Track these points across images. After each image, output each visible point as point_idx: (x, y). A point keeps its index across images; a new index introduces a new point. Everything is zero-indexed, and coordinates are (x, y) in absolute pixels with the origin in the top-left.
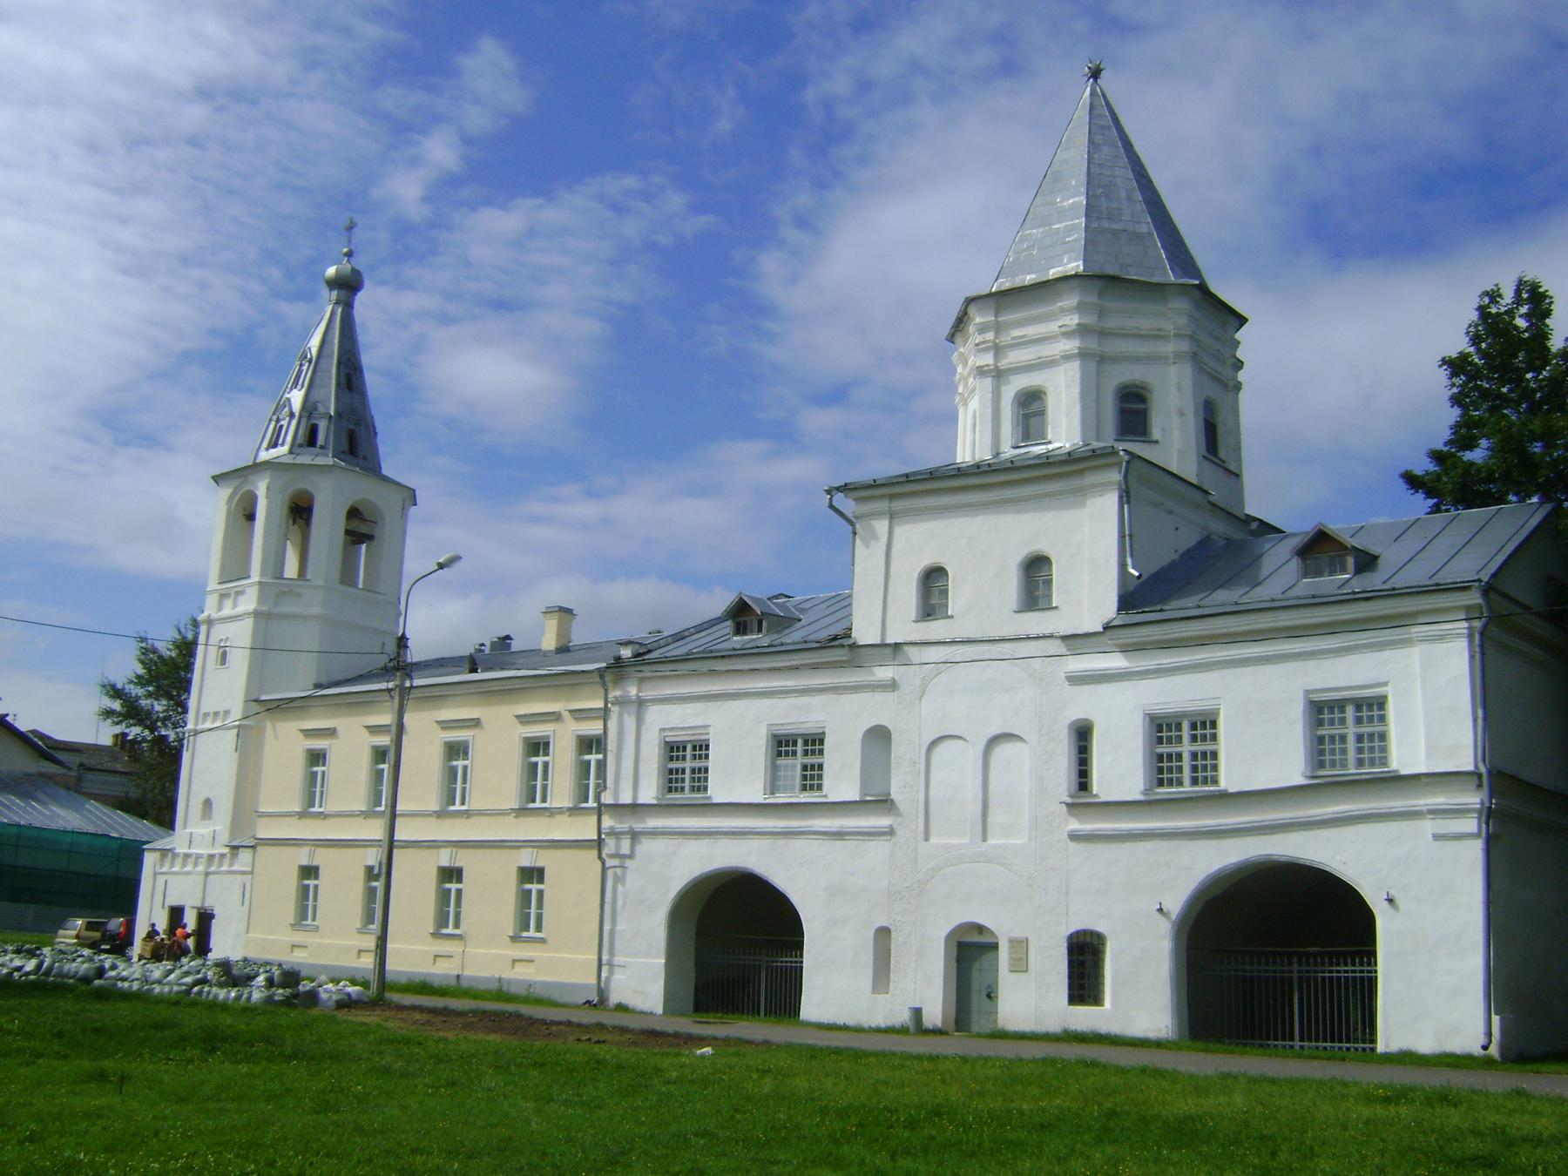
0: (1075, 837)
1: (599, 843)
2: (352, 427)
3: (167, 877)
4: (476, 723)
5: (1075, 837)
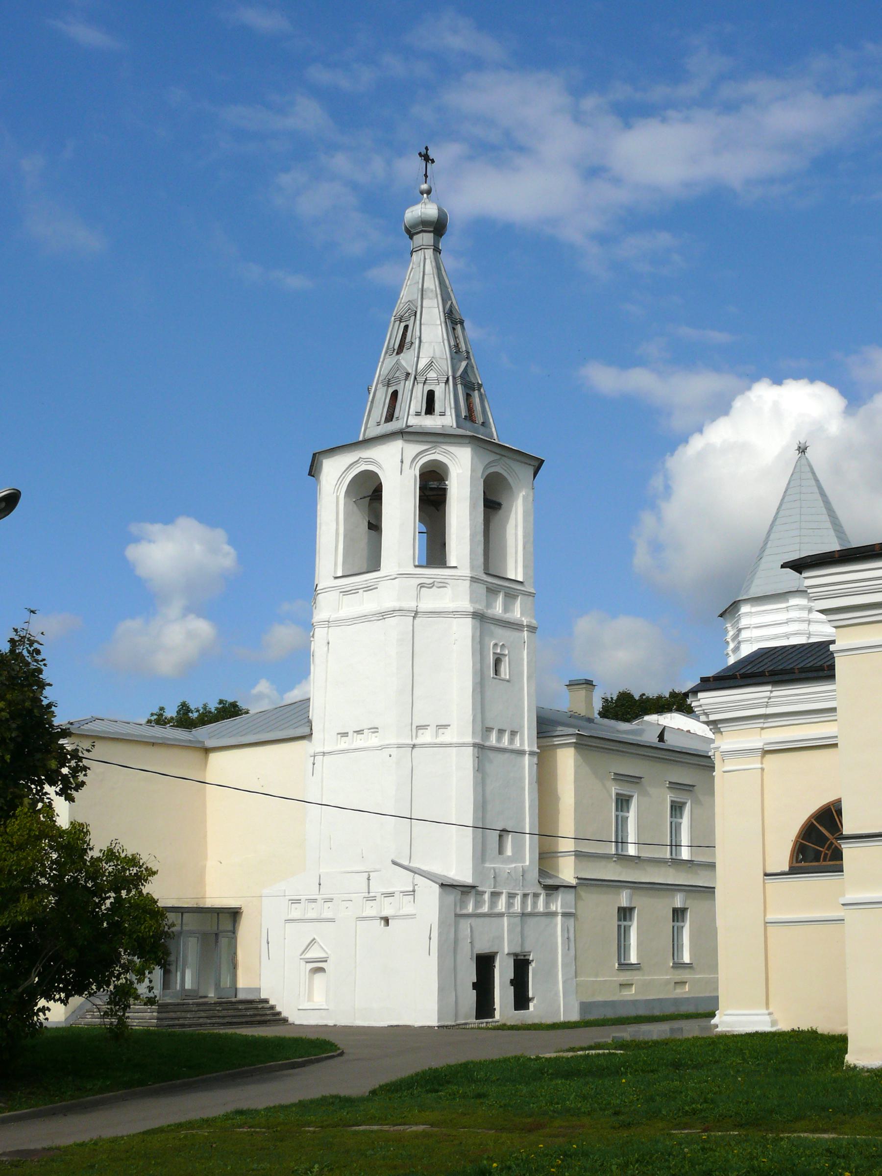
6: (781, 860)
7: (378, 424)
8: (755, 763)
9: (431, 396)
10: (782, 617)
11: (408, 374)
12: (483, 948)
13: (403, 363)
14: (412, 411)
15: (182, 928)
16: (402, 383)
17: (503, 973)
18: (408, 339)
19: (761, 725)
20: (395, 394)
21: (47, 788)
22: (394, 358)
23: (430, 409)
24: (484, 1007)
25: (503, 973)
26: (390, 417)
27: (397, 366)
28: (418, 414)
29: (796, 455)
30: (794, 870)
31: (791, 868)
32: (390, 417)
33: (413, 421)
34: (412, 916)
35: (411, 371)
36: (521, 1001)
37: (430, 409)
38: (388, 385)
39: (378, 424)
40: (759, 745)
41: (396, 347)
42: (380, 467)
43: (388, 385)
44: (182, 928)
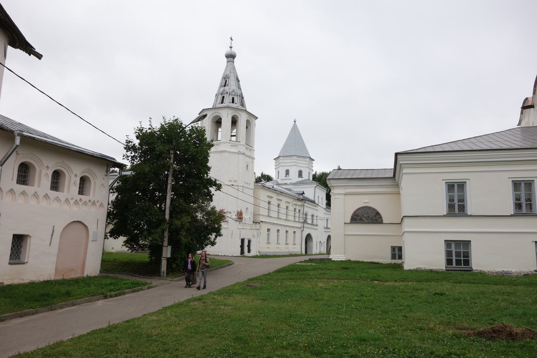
0: (325, 231)
5: (325, 231)
6: (348, 221)
7: (219, 104)
8: (343, 197)
9: (233, 98)
10: (290, 161)
11: (227, 92)
12: (242, 237)
13: (225, 89)
14: (229, 102)
15: (304, 225)
16: (226, 94)
17: (246, 243)
18: (227, 84)
19: (345, 188)
20: (223, 97)
21: (210, 189)
22: (224, 88)
23: (233, 102)
24: (242, 252)
25: (246, 243)
26: (222, 102)
27: (224, 90)
28: (230, 103)
29: (293, 123)
30: (351, 223)
31: (350, 222)
32: (222, 102)
33: (229, 104)
34: (227, 228)
35: (228, 92)
36: (249, 251)
37: (233, 102)
38: (222, 94)
39: (219, 104)
40: (344, 192)
41: (224, 85)
42: (222, 115)
43: (222, 94)
44: (304, 225)
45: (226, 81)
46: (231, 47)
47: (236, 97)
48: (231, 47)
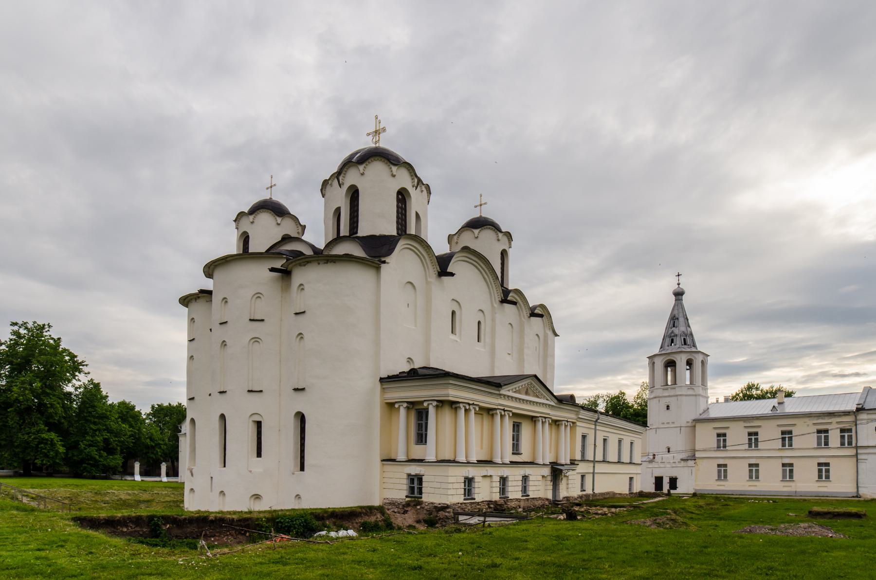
1: (857, 454)
2: (684, 337)
3: (653, 469)
4: (759, 427)
23: (685, 344)
28: (682, 345)
45: (674, 322)
46: (679, 284)
47: (688, 337)
48: (679, 284)
